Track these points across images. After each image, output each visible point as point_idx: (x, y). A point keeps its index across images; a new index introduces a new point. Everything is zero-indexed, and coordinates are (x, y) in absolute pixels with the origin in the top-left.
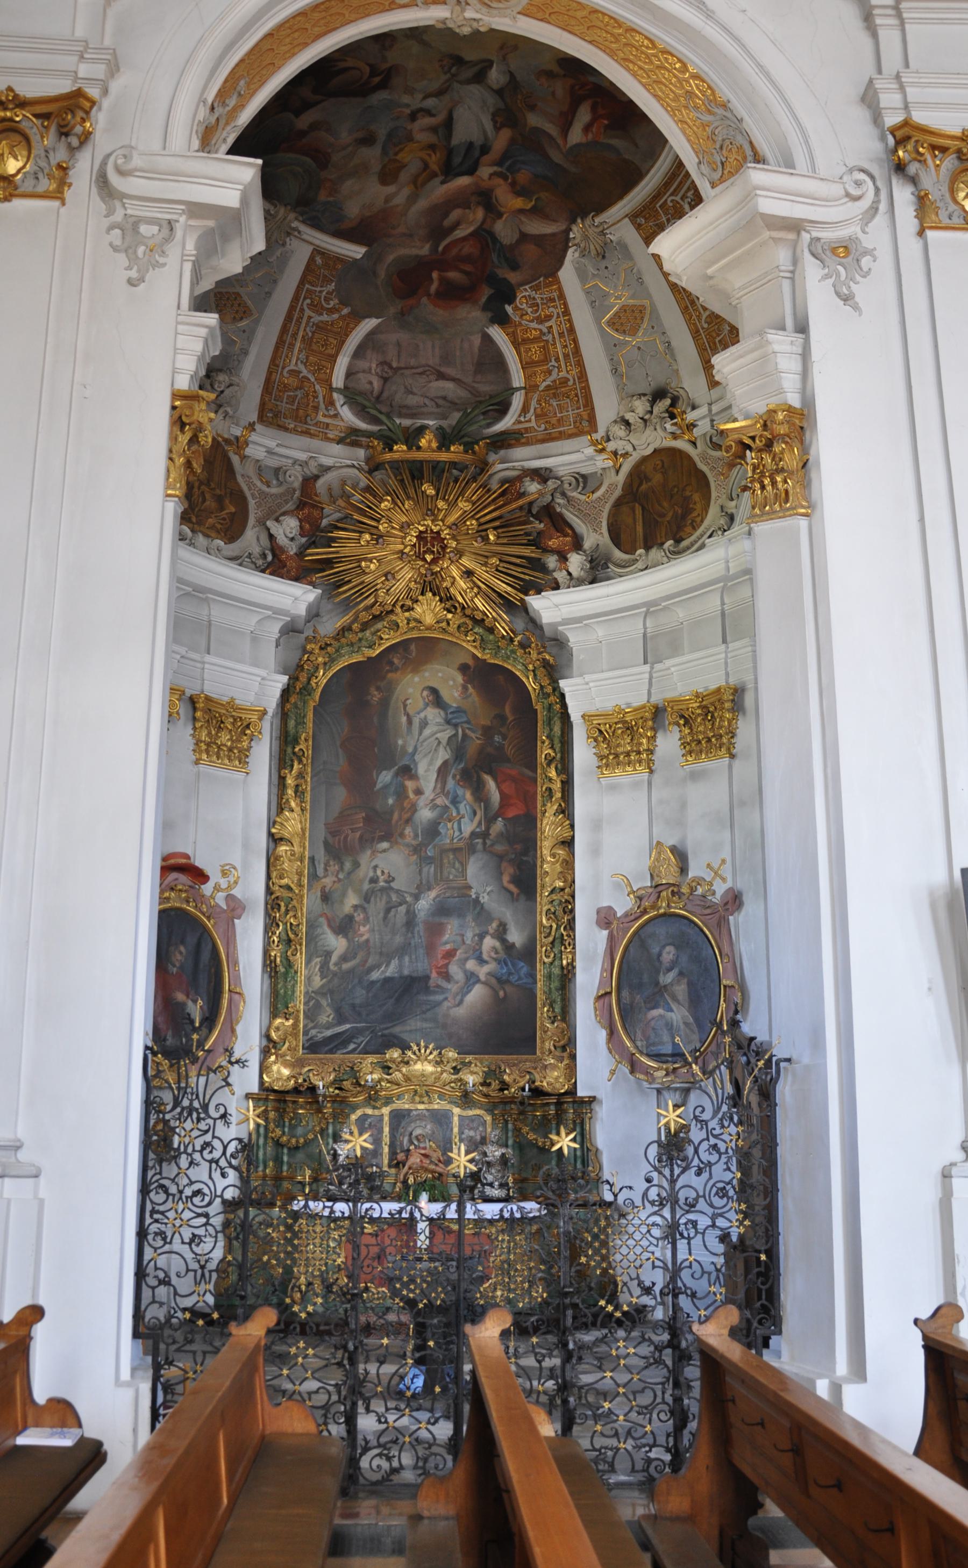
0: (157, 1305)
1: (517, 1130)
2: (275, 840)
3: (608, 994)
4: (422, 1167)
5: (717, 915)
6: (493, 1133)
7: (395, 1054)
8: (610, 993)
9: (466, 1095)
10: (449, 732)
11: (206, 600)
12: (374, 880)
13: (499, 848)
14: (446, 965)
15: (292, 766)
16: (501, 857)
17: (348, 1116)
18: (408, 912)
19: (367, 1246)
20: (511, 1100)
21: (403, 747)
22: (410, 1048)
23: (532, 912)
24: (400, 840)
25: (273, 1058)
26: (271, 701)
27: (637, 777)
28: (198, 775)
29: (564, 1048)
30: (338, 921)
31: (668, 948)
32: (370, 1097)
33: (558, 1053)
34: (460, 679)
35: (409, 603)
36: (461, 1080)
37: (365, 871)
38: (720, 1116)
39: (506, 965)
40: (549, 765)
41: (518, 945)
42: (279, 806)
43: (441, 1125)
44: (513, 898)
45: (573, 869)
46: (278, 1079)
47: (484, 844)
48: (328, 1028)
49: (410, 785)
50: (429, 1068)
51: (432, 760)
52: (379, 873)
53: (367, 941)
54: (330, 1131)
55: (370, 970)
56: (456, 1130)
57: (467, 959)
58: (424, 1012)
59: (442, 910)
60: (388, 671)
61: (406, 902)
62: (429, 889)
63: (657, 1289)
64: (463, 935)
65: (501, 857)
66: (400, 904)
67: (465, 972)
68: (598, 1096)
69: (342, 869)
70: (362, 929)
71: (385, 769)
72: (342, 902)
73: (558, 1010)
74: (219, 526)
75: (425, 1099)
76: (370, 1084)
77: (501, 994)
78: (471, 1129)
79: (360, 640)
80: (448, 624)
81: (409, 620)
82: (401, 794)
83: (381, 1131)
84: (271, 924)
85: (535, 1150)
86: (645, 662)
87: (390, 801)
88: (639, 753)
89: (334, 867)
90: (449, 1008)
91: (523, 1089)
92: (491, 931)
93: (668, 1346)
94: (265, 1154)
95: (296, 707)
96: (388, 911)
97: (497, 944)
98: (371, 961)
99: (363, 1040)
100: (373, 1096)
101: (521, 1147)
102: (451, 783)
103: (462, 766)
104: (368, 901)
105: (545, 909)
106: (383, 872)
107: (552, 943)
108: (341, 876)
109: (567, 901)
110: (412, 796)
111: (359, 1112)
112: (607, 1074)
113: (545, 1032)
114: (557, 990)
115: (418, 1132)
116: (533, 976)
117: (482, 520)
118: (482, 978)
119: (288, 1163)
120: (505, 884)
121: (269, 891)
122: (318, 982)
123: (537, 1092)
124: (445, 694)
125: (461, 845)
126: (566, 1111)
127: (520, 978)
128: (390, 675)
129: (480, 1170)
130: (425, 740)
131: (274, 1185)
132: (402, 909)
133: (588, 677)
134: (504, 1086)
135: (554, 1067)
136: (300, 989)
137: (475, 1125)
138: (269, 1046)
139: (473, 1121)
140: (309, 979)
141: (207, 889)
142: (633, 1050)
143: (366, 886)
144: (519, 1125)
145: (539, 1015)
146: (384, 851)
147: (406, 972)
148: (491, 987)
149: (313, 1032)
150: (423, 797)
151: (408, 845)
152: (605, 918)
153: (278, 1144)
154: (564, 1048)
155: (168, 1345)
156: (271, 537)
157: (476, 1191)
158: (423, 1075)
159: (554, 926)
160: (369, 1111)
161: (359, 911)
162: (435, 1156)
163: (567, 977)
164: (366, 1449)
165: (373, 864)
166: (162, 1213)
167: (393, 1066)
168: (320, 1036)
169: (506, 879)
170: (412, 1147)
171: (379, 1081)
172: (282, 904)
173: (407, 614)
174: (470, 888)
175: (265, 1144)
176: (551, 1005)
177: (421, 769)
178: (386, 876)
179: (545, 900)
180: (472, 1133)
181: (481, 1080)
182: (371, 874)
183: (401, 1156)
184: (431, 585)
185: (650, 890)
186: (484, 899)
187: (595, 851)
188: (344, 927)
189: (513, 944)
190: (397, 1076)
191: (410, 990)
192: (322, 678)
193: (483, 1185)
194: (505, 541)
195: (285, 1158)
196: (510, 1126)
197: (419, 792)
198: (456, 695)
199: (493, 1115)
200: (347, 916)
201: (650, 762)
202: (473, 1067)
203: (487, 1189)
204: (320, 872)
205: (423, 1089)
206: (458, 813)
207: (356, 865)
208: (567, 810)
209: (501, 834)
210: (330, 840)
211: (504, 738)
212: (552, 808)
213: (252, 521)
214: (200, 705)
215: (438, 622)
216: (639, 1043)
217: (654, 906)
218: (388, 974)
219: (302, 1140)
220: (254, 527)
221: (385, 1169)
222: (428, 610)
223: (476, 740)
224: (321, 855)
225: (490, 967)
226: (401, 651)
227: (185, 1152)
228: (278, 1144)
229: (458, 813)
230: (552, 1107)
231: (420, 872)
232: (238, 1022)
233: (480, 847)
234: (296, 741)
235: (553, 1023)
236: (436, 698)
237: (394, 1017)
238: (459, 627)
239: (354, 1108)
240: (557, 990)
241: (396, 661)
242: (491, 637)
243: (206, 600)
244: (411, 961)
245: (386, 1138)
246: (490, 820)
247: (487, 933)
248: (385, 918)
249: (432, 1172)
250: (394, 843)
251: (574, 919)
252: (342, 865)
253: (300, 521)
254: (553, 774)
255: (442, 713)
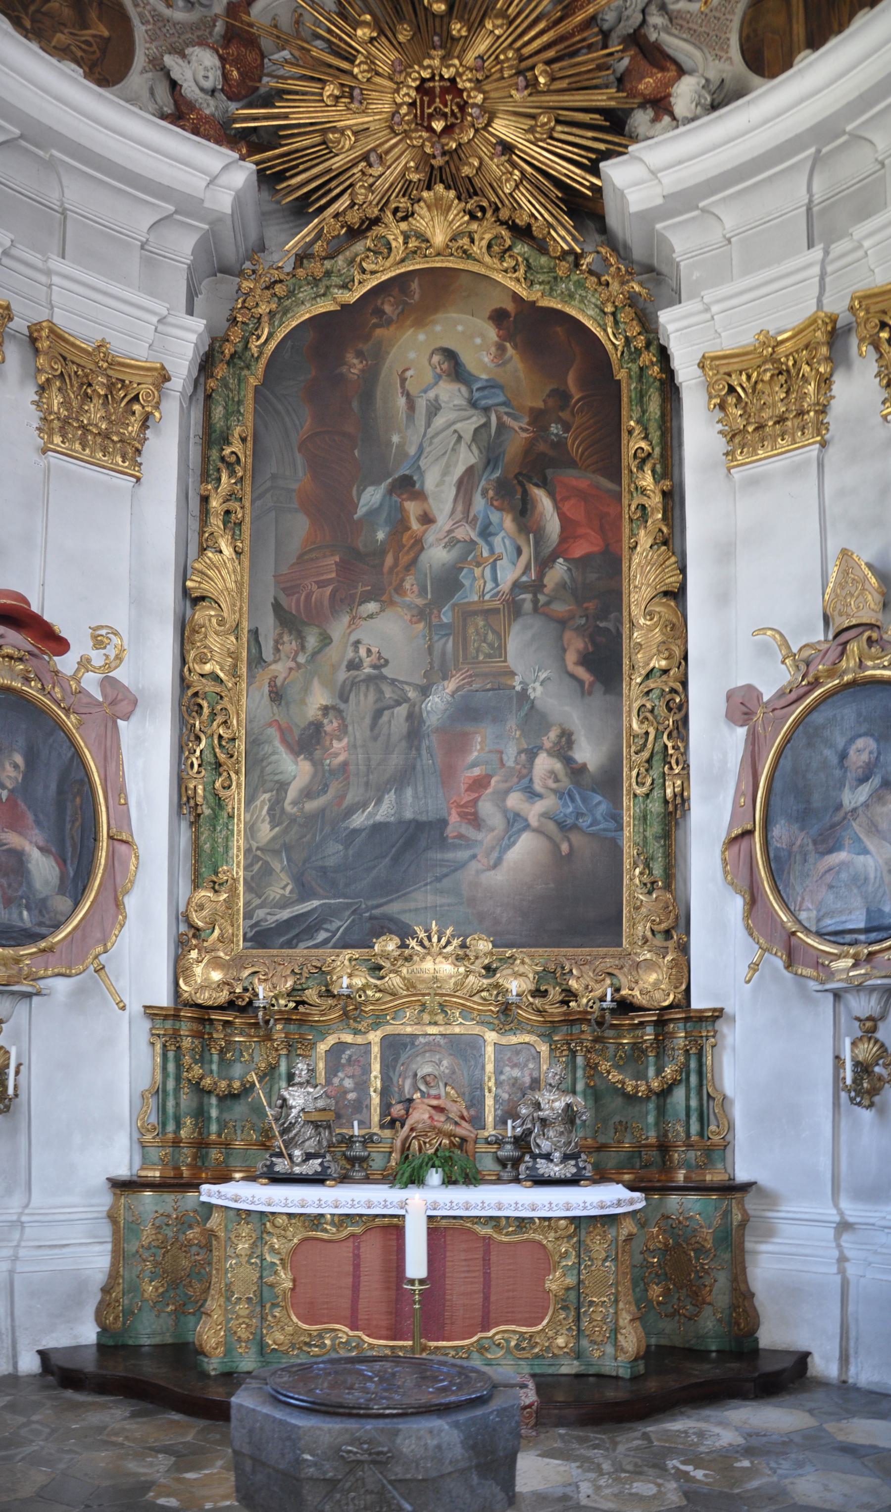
1: (592, 1067)
2: (192, 599)
3: (749, 833)
6: (550, 1070)
7: (389, 945)
9: (506, 1009)
10: (477, 420)
11: (50, 165)
12: (354, 665)
13: (560, 608)
14: (475, 801)
15: (219, 480)
16: (562, 623)
17: (313, 1045)
18: (410, 716)
20: (582, 1018)
21: (401, 446)
22: (414, 935)
23: (617, 712)
24: (397, 598)
25: (194, 954)
26: (182, 364)
27: (798, 456)
28: (48, 470)
29: (667, 934)
30: (296, 733)
31: (860, 743)
32: (346, 1014)
33: (659, 941)
34: (492, 333)
35: (404, 203)
36: (497, 986)
37: (338, 652)
39: (573, 800)
40: (641, 468)
41: (591, 767)
42: (196, 538)
43: (466, 1060)
44: (584, 691)
46: (202, 988)
47: (535, 602)
48: (284, 907)
49: (412, 508)
50: (446, 968)
51: (448, 466)
52: (363, 652)
53: (345, 764)
54: (283, 1068)
55: (350, 812)
56: (490, 1067)
57: (507, 791)
58: (438, 879)
59: (466, 712)
60: (376, 326)
61: (407, 700)
62: (445, 677)
64: (501, 753)
65: (562, 623)
66: (398, 703)
67: (505, 811)
68: (728, 1010)
69: (303, 648)
70: (336, 744)
71: (372, 484)
72: (303, 702)
73: (658, 870)
74: (79, 54)
75: (440, 1018)
77: (565, 848)
79: (328, 274)
80: (472, 241)
81: (407, 238)
82: (400, 525)
83: (367, 1070)
84: (185, 737)
85: (619, 1100)
86: (810, 245)
87: (381, 535)
88: (801, 413)
89: (290, 644)
90: (478, 872)
91: (602, 999)
92: (548, 744)
94: (177, 1105)
95: (226, 386)
96: (378, 714)
97: (558, 766)
99: (340, 925)
100: (351, 1010)
101: (597, 1095)
102: (479, 503)
103: (497, 474)
104: (346, 700)
105: (636, 705)
106: (369, 651)
107: (649, 761)
108: (301, 659)
109: (673, 691)
110: (415, 525)
111: (331, 1040)
112: (743, 971)
113: (637, 908)
114: (657, 838)
115: (426, 1069)
116: (616, 818)
117: (526, 51)
118: (534, 821)
119: (218, 1119)
120: (571, 667)
122: (266, 832)
123: (625, 1006)
124: (468, 360)
125: (497, 604)
126: (672, 1035)
127: (595, 822)
128: (379, 332)
129: (529, 1132)
130: (433, 437)
131: (195, 1158)
132: (402, 711)
133: (709, 295)
134: (569, 995)
135: (651, 965)
136: (238, 843)
137: (522, 1059)
138: (187, 937)
139: (518, 1053)
140: (251, 830)
141: (66, 664)
142: (791, 926)
143: (342, 675)
145: (626, 881)
146: (371, 616)
147: (408, 815)
148: (549, 838)
150: (433, 527)
151: (409, 607)
152: (742, 706)
153: (201, 1091)
154: (667, 934)
156: (174, 85)
157: (522, 1167)
158: (436, 979)
159: (652, 731)
161: (331, 714)
162: (454, 1110)
163: (675, 812)
165: (353, 638)
167: (387, 964)
168: (271, 919)
169: (571, 658)
170: (417, 1096)
171: (363, 989)
172: (205, 704)
173: (404, 226)
174: (513, 674)
175: (177, 1090)
176: (647, 865)
177: (430, 481)
178: (374, 657)
180: (516, 1073)
181: (532, 987)
182: (350, 654)
183: (397, 1110)
184: (443, 172)
185: (824, 647)
186: (536, 692)
187: (723, 597)
188: (308, 741)
189: (583, 768)
190: (394, 981)
191: (415, 842)
192: (267, 341)
193: (534, 1157)
194: (563, 84)
195: (214, 1113)
196: (580, 1060)
197: (427, 519)
198: (486, 360)
199: (551, 1042)
200: (311, 723)
201: (820, 427)
204: (268, 653)
205: (437, 1002)
206: (492, 551)
207: (326, 640)
208: (671, 540)
209: (562, 585)
210: (284, 602)
211: (567, 427)
212: (644, 539)
213: (140, 60)
214: (44, 345)
215: (453, 239)
216: (803, 916)
217: (831, 673)
218: (379, 818)
219: (237, 1084)
220: (144, 71)
221: (375, 1129)
222: (438, 224)
223: (520, 431)
224: (269, 626)
225: (548, 803)
226: (396, 292)
228: (201, 1091)
229: (492, 551)
230: (649, 1029)
231: (430, 649)
232: (127, 892)
233: (528, 606)
234: (226, 440)
235: (650, 893)
236: (453, 366)
237: (390, 888)
238: (489, 246)
240: (657, 838)
241: (387, 308)
242: (543, 260)
243: (50, 165)
244: (415, 796)
246: (544, 563)
247: (540, 748)
248: (374, 725)
249: (450, 1135)
250: (387, 604)
251: (685, 720)
252: (301, 638)
253: (222, 58)
254: (647, 480)
255: (464, 389)
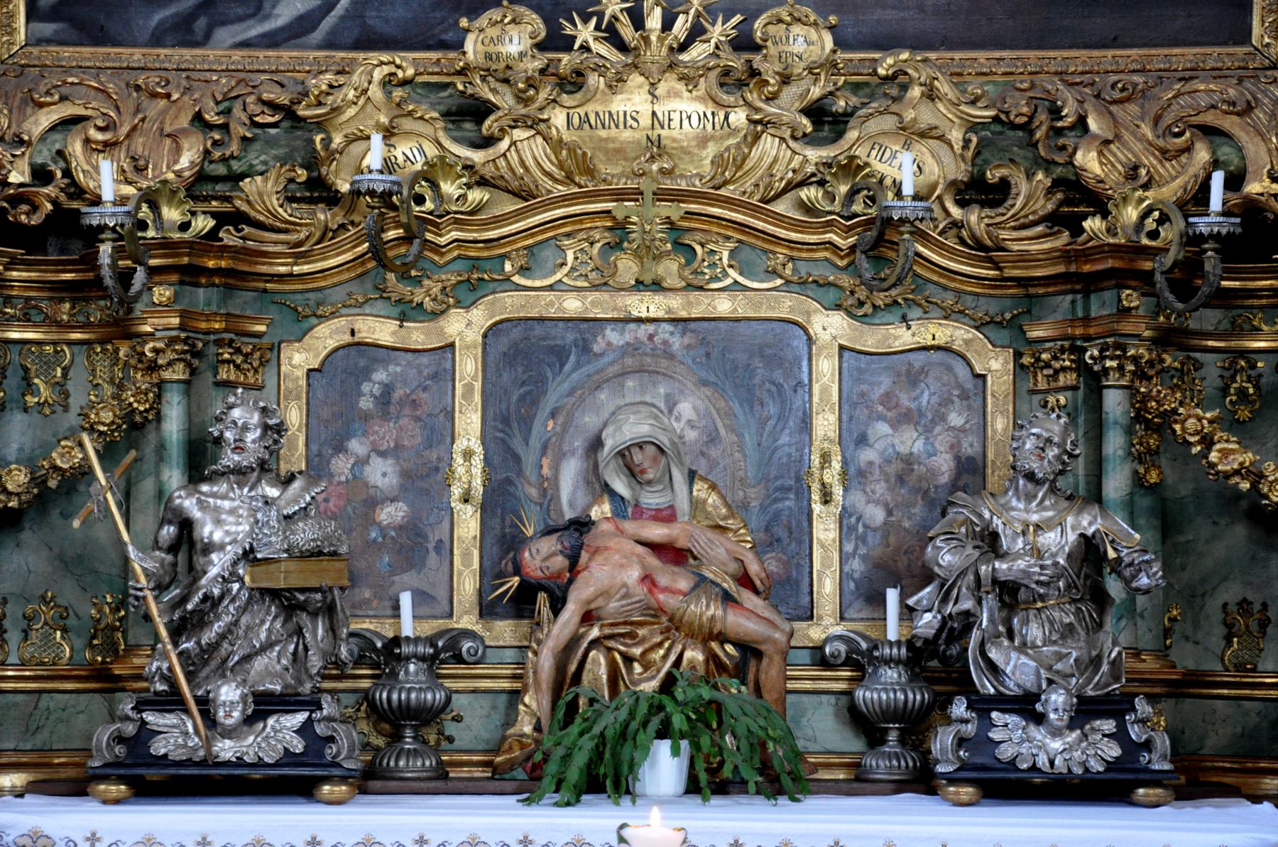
1: (1151, 425)
4: (656, 612)
17: (269, 353)
20: (1127, 266)
36: (850, 168)
43: (750, 400)
54: (173, 424)
56: (825, 425)
75: (670, 269)
76: (380, 183)
78: (905, 418)
100: (397, 242)
115: (633, 428)
134: (1080, 197)
139: (913, 379)
144: (1163, 396)
157: (942, 741)
160: (381, 330)
162: (720, 556)
167: (504, 100)
171: (429, 176)
180: (910, 441)
181: (959, 171)
183: (542, 556)
190: (525, 151)
193: (982, 706)
196: (1115, 402)
202: (919, 113)
203: (1008, 731)
205: (667, 219)
221: (467, 620)
239: (302, 320)
245: (469, 472)
249: (709, 635)
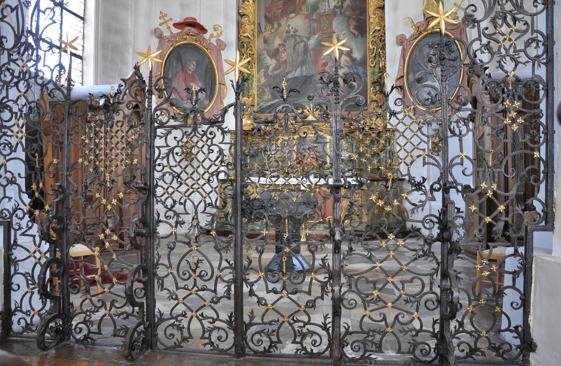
0: (7, 200)
2: (241, 15)
3: (402, 77)
5: (460, 29)
8: (403, 77)
12: (288, 32)
13: (348, 13)
16: (349, 17)
18: (304, 46)
19: (158, 147)
22: (306, 108)
23: (365, 43)
24: (300, 12)
30: (271, 52)
38: (493, 15)
39: (352, 68)
41: (358, 59)
44: (355, 37)
45: (384, 20)
47: (341, 11)
48: (268, 102)
52: (290, 28)
53: (286, 60)
55: (287, 74)
61: (303, 41)
63: (427, 185)
65: (349, 17)
66: (301, 42)
69: (273, 27)
70: (283, 55)
72: (273, 43)
89: (269, 26)
93: (438, 240)
96: (295, 46)
97: (348, 59)
98: (287, 70)
104: (286, 42)
105: (371, 40)
106: (292, 28)
107: (375, 57)
108: (273, 31)
109: (382, 36)
120: (351, 30)
121: (239, 39)
122: (263, 80)
132: (302, 44)
136: (255, 84)
140: (259, 80)
141: (207, 36)
143: (284, 35)
145: (368, 92)
146: (293, 18)
147: (304, 74)
149: (262, 104)
152: (401, 40)
155: (16, 230)
159: (375, 48)
164: (162, 320)
165: (288, 24)
166: (9, 128)
168: (265, 105)
169: (351, 27)
172: (245, 45)
179: (371, 36)
182: (287, 29)
188: (275, 54)
189: (356, 59)
204: (263, 30)
207: (280, 25)
209: (349, 6)
210: (267, 15)
217: (425, 30)
218: (296, 75)
224: (263, 22)
227: (24, 79)
233: (339, 13)
235: (375, 95)
244: (306, 69)
250: (297, 14)
252: (273, 25)
